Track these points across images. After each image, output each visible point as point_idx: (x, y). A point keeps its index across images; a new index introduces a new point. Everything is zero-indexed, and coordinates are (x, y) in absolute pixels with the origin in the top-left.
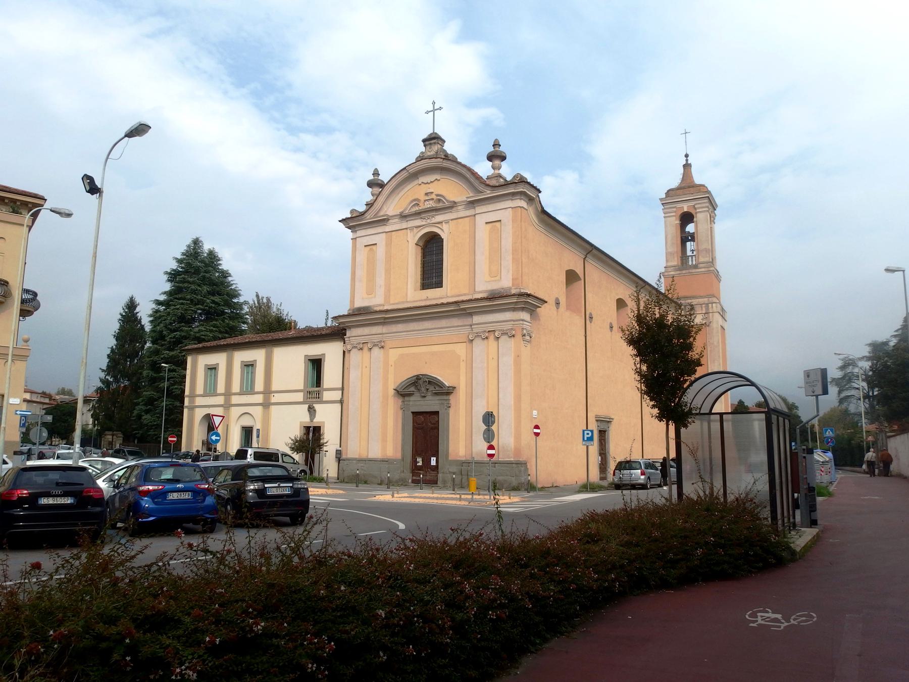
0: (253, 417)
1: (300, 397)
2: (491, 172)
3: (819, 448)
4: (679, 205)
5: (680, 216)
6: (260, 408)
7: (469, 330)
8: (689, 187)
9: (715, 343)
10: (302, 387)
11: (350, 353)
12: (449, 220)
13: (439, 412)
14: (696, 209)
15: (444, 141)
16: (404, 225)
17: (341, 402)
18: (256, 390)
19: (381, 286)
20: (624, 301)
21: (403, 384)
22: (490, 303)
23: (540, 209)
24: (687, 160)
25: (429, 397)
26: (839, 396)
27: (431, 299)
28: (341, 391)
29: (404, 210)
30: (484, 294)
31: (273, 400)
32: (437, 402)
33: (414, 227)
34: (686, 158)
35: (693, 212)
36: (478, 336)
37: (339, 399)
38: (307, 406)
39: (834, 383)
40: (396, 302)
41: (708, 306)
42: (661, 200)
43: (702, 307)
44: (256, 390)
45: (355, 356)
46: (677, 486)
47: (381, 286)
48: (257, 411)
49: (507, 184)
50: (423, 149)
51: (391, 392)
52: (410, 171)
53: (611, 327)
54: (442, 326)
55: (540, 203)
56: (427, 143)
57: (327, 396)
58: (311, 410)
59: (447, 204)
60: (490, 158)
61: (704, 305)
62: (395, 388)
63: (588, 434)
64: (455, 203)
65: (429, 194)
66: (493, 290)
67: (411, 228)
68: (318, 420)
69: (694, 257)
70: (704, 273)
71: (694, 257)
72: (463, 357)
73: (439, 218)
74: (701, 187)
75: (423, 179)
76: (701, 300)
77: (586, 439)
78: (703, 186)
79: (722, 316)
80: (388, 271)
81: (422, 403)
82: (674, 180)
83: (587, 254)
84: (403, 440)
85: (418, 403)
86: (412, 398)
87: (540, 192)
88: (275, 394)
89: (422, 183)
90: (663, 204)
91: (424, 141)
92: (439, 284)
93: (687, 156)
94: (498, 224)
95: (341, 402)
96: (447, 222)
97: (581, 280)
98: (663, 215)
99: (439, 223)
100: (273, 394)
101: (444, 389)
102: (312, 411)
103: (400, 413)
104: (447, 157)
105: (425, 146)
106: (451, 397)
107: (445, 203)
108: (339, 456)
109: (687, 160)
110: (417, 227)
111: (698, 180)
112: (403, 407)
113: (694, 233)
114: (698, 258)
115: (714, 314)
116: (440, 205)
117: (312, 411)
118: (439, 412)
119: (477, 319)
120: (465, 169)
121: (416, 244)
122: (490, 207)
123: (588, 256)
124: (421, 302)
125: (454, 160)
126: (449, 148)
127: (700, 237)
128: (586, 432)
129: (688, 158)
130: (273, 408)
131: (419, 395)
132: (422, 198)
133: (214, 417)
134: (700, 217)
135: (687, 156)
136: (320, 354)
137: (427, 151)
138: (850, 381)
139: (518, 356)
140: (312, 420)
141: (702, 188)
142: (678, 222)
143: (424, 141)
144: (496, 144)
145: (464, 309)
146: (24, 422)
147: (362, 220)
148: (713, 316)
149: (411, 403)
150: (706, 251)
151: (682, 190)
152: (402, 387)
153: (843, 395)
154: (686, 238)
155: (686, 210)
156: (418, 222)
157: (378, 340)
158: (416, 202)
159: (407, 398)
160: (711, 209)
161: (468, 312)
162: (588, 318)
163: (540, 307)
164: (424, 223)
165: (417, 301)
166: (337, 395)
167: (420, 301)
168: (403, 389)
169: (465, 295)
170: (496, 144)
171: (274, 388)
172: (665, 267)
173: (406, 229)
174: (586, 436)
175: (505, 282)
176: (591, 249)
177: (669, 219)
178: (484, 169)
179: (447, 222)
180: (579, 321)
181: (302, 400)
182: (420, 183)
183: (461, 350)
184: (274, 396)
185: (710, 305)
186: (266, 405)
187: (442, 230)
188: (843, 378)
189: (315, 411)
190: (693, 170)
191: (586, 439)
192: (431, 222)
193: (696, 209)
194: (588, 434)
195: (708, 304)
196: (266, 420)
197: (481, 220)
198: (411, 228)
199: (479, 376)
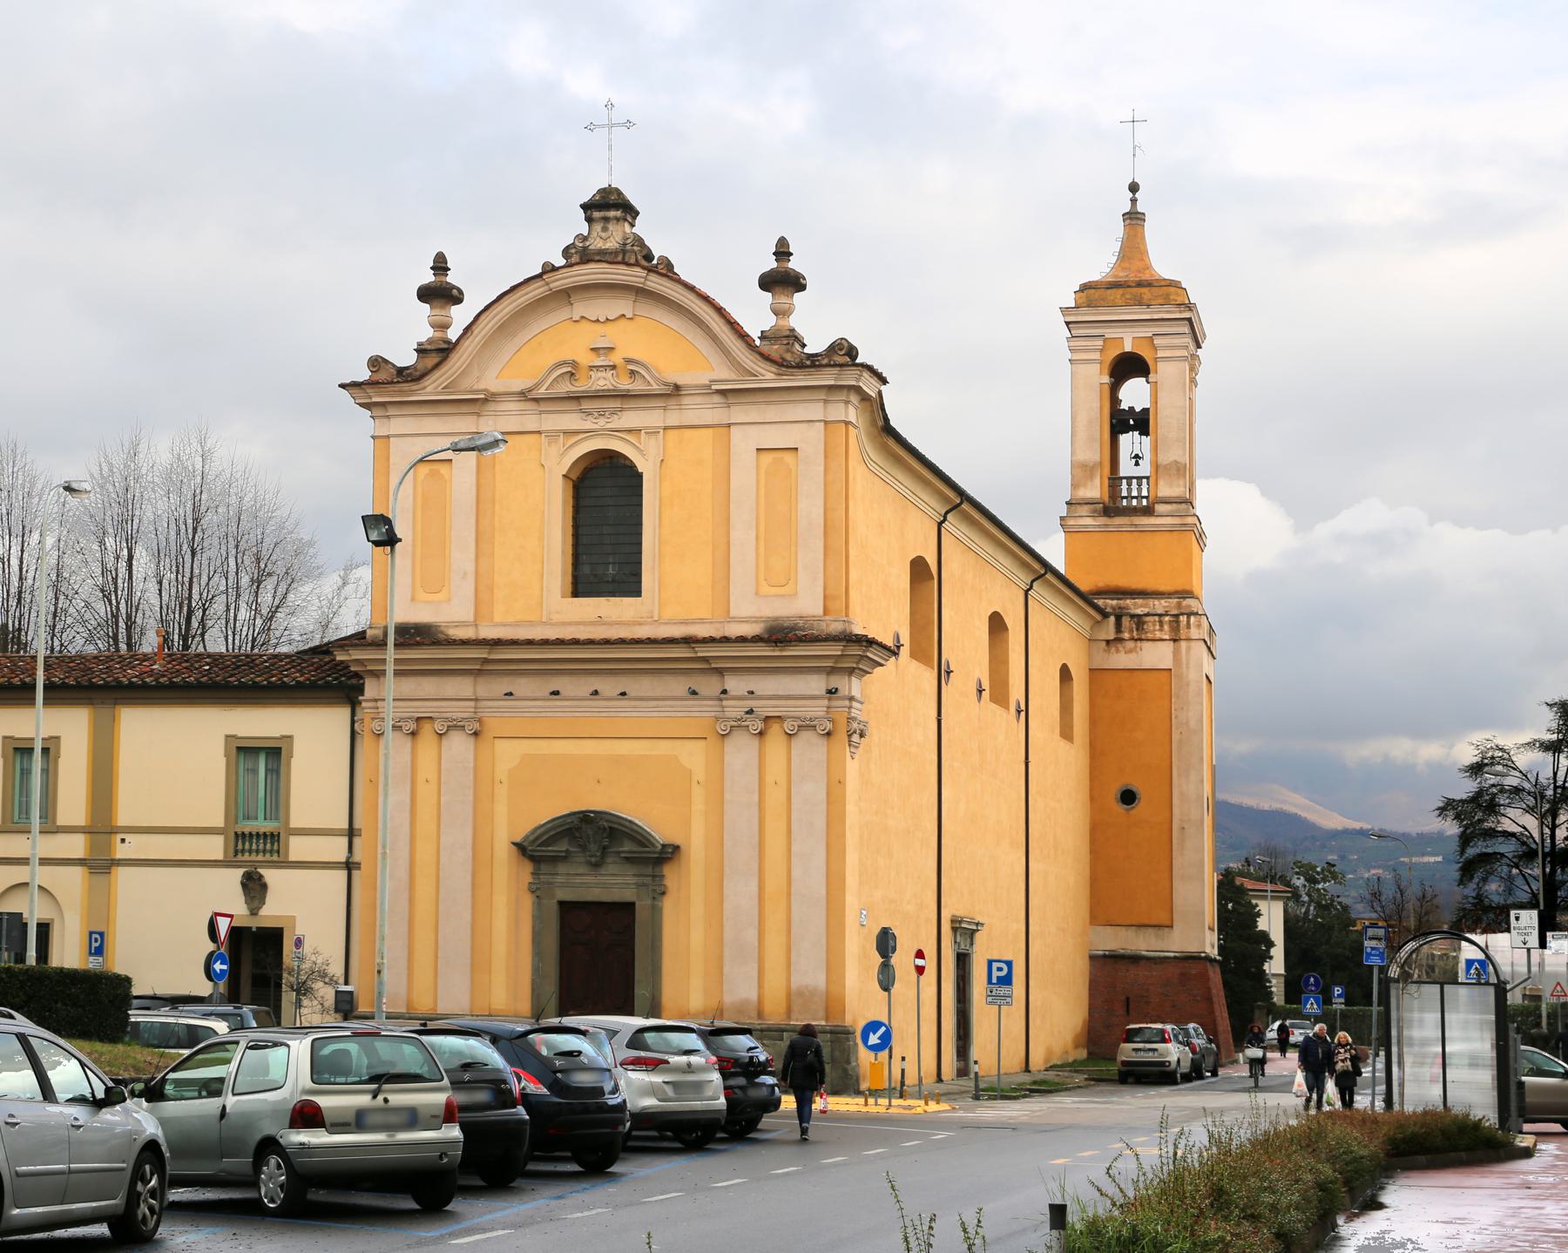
0: (57, 902)
1: (215, 847)
2: (768, 322)
3: (261, 815)
4: (1111, 333)
5: (1110, 365)
6: (78, 872)
7: (718, 709)
8: (1140, 284)
9: (1192, 723)
10: (218, 821)
11: (378, 740)
12: (659, 427)
13: (633, 904)
14: (1155, 349)
15: (637, 213)
16: (531, 423)
17: (350, 866)
18: (59, 823)
19: (465, 574)
20: (1001, 616)
21: (539, 832)
22: (774, 651)
23: (880, 423)
24: (1134, 201)
25: (611, 868)
26: (1462, 852)
27: (611, 624)
28: (345, 840)
29: (537, 386)
30: (754, 625)
31: (121, 852)
32: (632, 880)
33: (559, 431)
34: (1131, 195)
35: (1146, 354)
36: (739, 726)
37: (344, 860)
38: (237, 874)
39: (1451, 814)
40: (510, 619)
41: (1178, 622)
42: (1065, 311)
43: (1161, 623)
44: (59, 823)
45: (393, 753)
46: (757, 1125)
47: (465, 574)
48: (71, 883)
49: (813, 363)
50: (584, 228)
51: (503, 851)
52: (552, 285)
53: (980, 691)
54: (642, 694)
55: (883, 409)
56: (596, 214)
57: (298, 848)
58: (251, 885)
59: (656, 387)
60: (768, 282)
61: (1167, 618)
62: (518, 840)
63: (1000, 969)
64: (677, 387)
65: (602, 352)
66: (776, 619)
67: (553, 435)
68: (272, 911)
69: (1144, 481)
70: (1171, 531)
71: (1144, 481)
72: (699, 774)
73: (630, 419)
74: (1172, 289)
75: (581, 308)
76: (1160, 605)
77: (994, 981)
78: (1175, 285)
79: (1209, 648)
80: (482, 539)
81: (590, 879)
82: (1100, 263)
83: (1032, 582)
84: (537, 971)
85: (578, 880)
86: (562, 868)
87: (884, 381)
88: (128, 837)
89: (583, 317)
90: (1068, 323)
91: (585, 207)
92: (627, 583)
93: (1134, 188)
94: (788, 457)
95: (350, 866)
96: (652, 432)
97: (933, 578)
98: (1069, 355)
99: (629, 431)
100: (123, 836)
101: (652, 849)
102: (254, 887)
103: (528, 901)
104: (640, 255)
105: (589, 220)
106: (668, 871)
107: (652, 386)
108: (347, 1007)
109: (1134, 201)
110: (568, 433)
111: (1163, 265)
112: (534, 887)
113: (1146, 411)
114: (1157, 484)
115: (1193, 644)
116: (637, 386)
117: (254, 887)
118: (633, 904)
119: (735, 684)
120: (692, 296)
121: (564, 476)
122: (772, 412)
123: (1035, 584)
124: (582, 628)
125: (666, 269)
126: (654, 232)
127: (1163, 422)
128: (995, 965)
129: (1137, 195)
130: (122, 874)
131: (582, 860)
132: (586, 359)
133: (218, 918)
134: (1165, 371)
135: (1134, 188)
136: (278, 735)
137: (594, 234)
138: (1492, 808)
139: (840, 782)
140: (254, 912)
141: (1169, 289)
142: (1106, 379)
143: (585, 207)
144: (782, 252)
145: (705, 660)
146: (97, 944)
147: (412, 392)
148: (1189, 649)
149: (559, 879)
150: (1178, 470)
151: (1121, 291)
152: (537, 839)
153: (1471, 852)
154: (1124, 421)
155: (1128, 348)
156: (571, 421)
157: (465, 715)
158: (572, 370)
159: (544, 868)
160: (1192, 346)
161: (713, 666)
162: (943, 673)
163: (882, 665)
164: (588, 425)
165: (570, 624)
166: (336, 849)
167: (578, 623)
168: (539, 846)
169: (702, 621)
170: (782, 252)
171: (123, 818)
172: (1067, 503)
173: (539, 432)
174: (995, 974)
175: (804, 603)
176: (1043, 572)
177: (1082, 368)
178: (756, 314)
179: (652, 432)
180: (929, 677)
181: (220, 857)
182: (576, 317)
183: (693, 756)
184: (123, 840)
185: (1183, 619)
186: (100, 865)
187: (640, 451)
188: (1476, 798)
189: (264, 887)
190: (1150, 229)
191: (994, 981)
192: (609, 426)
193: (1155, 349)
194: (1000, 969)
195: (1177, 616)
196: (100, 904)
197: (744, 442)
198: (553, 435)
199: (740, 819)
